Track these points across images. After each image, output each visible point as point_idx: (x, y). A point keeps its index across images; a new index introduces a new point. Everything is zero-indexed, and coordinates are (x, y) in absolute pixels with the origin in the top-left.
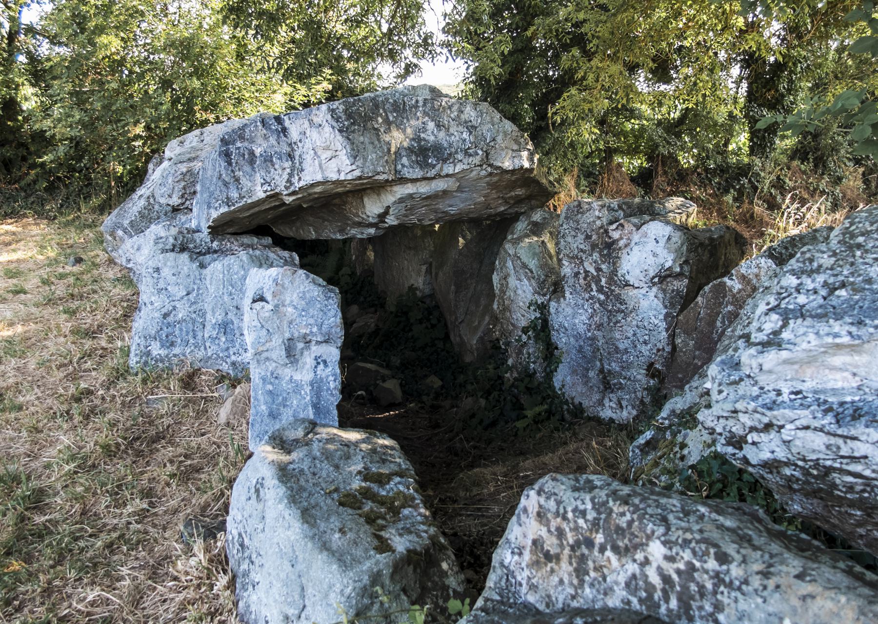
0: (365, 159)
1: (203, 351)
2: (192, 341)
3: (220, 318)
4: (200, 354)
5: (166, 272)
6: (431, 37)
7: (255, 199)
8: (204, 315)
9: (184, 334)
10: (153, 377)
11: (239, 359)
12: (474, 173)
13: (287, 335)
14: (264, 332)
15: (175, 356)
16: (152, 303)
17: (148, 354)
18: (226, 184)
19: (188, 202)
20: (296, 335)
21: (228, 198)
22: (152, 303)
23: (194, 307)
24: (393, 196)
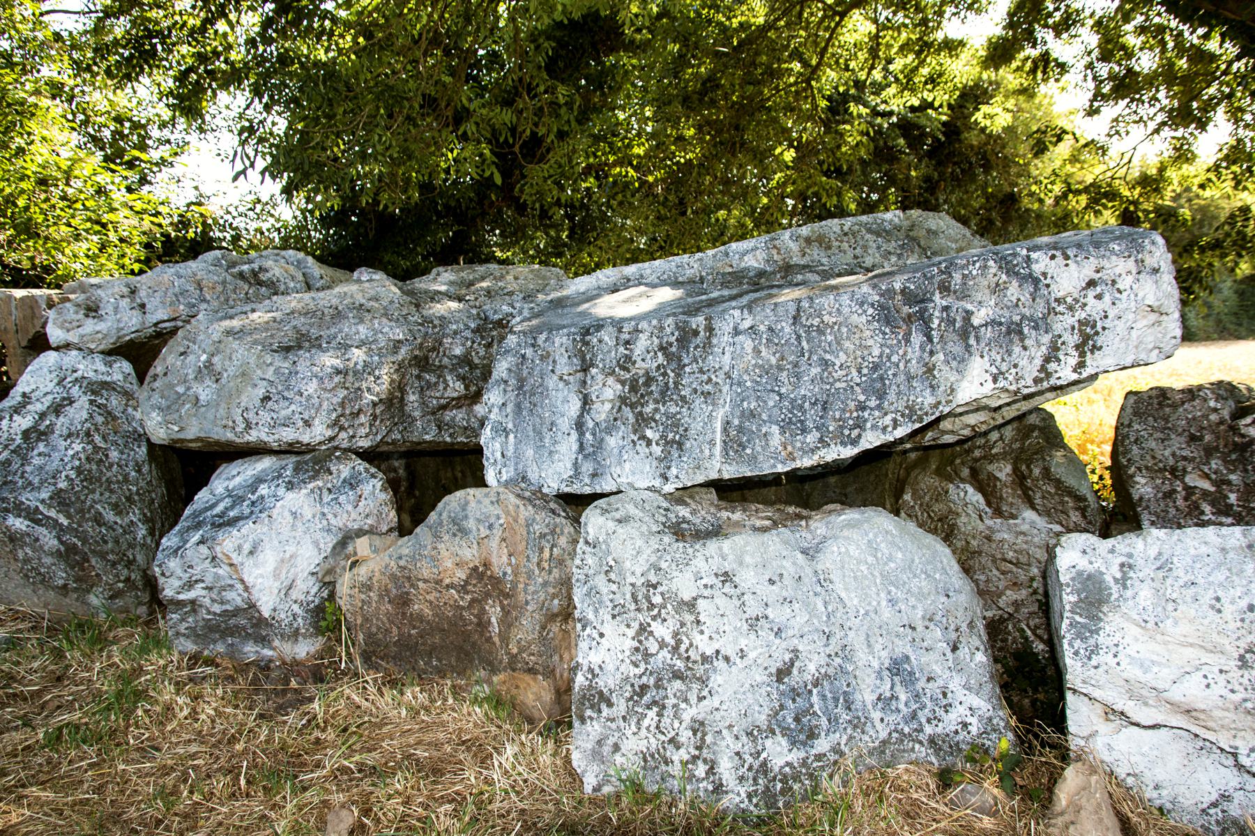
2: (845, 717)
11: (939, 730)
15: (819, 757)
16: (742, 654)
19: (343, 435)
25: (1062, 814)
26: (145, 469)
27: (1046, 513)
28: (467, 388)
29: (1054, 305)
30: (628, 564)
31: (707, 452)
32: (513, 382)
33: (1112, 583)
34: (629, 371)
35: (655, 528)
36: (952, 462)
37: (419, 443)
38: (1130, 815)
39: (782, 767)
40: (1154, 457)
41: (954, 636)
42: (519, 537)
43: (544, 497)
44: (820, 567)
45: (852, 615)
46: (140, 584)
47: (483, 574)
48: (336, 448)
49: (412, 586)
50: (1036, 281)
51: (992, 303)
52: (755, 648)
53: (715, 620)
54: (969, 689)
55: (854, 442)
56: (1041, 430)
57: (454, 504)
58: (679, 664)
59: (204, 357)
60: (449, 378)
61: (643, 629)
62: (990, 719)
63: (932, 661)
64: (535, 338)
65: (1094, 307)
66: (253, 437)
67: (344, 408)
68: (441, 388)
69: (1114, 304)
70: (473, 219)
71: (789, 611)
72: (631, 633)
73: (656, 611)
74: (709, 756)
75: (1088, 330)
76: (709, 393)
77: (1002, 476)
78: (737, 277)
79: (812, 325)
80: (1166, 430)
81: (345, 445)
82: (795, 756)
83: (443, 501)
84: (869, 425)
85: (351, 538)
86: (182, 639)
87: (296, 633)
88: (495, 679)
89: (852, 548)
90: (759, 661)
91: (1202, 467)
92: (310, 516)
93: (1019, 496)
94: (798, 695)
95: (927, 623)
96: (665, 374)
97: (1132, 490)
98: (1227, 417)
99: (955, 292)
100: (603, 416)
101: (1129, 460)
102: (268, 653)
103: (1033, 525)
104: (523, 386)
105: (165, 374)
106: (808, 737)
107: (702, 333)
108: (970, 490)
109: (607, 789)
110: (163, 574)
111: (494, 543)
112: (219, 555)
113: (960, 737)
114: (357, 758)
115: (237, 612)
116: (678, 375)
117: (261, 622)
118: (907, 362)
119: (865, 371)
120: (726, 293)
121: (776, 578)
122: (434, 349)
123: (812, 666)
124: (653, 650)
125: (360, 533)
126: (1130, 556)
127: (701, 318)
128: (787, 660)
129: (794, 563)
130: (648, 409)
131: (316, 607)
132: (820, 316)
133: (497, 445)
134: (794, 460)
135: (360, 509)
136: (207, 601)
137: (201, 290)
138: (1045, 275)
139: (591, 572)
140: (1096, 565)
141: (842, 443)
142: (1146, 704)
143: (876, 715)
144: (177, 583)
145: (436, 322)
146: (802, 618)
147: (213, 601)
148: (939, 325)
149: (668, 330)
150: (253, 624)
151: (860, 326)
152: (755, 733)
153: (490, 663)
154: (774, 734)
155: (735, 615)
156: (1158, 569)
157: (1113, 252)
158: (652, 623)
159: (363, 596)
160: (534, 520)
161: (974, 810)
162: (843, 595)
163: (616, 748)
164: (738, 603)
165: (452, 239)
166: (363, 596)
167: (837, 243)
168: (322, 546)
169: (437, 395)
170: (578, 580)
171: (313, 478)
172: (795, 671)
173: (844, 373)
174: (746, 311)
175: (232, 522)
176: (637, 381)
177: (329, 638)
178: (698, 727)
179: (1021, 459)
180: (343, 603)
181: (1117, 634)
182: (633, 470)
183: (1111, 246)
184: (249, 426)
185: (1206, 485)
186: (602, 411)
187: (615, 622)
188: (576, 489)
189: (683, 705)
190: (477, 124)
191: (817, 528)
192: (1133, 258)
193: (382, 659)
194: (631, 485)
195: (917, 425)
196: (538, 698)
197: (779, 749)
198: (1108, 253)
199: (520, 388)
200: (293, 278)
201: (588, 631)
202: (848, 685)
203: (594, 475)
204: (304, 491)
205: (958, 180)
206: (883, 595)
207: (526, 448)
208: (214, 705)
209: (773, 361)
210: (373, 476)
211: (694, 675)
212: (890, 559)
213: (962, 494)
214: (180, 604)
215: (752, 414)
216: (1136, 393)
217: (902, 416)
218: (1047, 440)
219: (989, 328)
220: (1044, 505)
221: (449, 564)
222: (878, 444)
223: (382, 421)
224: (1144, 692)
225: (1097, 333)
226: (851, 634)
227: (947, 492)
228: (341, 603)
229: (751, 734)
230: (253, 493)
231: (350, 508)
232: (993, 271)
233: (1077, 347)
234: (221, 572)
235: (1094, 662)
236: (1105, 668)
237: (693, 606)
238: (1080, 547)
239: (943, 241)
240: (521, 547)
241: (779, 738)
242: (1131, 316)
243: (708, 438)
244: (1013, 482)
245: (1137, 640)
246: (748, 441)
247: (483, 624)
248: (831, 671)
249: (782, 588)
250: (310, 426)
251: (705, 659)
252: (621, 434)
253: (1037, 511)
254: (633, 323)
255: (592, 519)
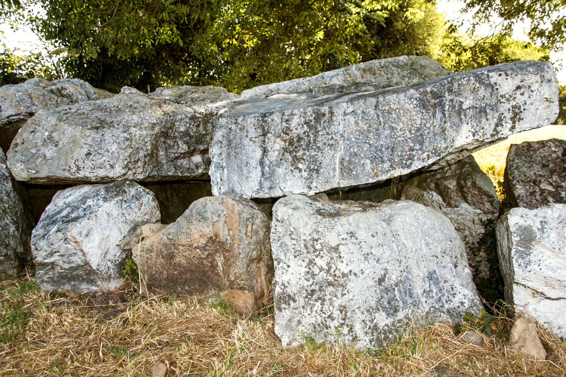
2: (410, 301)
11: (451, 306)
15: (399, 321)
17: (376, 327)
19: (130, 172)
25: (516, 342)
26: (12, 195)
27: (474, 204)
28: (189, 148)
29: (500, 98)
30: (301, 230)
31: (332, 174)
32: (225, 142)
33: (537, 231)
34: (288, 135)
35: (312, 212)
36: (426, 181)
37: (165, 177)
38: (548, 342)
39: (384, 327)
40: (525, 176)
41: (455, 260)
42: (234, 221)
43: (245, 200)
44: (393, 228)
45: (409, 251)
46: (13, 257)
47: (215, 240)
48: (126, 180)
49: (176, 248)
50: (492, 87)
51: (472, 98)
52: (368, 269)
53: (349, 256)
54: (463, 286)
55: (408, 167)
56: (470, 164)
57: (199, 205)
58: (331, 279)
59: (47, 134)
60: (180, 143)
61: (311, 262)
62: (473, 300)
63: (446, 273)
64: (236, 120)
65: (520, 99)
66: (81, 174)
67: (130, 158)
68: (176, 148)
69: (529, 97)
70: (153, 66)
71: (382, 250)
72: (304, 264)
73: (317, 253)
74: (350, 323)
75: (517, 110)
76: (332, 145)
77: (451, 187)
78: (330, 89)
79: (385, 110)
80: (531, 162)
81: (131, 178)
82: (389, 321)
83: (193, 204)
84: (416, 158)
85: (139, 226)
86: (45, 284)
87: (110, 277)
88: (222, 294)
89: (407, 219)
90: (370, 275)
91: (549, 179)
92: (116, 215)
93: (460, 196)
94: (389, 291)
95: (443, 254)
96: (308, 136)
97: (514, 192)
98: (560, 155)
99: (455, 92)
100: (274, 158)
101: (514, 177)
102: (94, 288)
103: (466, 210)
104: (230, 144)
105: (23, 143)
106: (394, 311)
107: (327, 115)
108: (435, 194)
109: (295, 344)
110: (36, 249)
111: (221, 224)
112: (69, 237)
113: (460, 309)
114: (157, 338)
115: (78, 267)
116: (316, 136)
117: (91, 272)
118: (434, 127)
119: (413, 132)
120: (326, 96)
121: (375, 234)
122: (171, 128)
123: (394, 277)
124: (316, 272)
125: (144, 223)
126: (545, 217)
127: (327, 107)
128: (383, 274)
129: (382, 227)
130: (300, 154)
131: (120, 263)
132: (389, 105)
133: (218, 175)
134: (377, 176)
135: (142, 210)
136: (61, 263)
137: (32, 99)
138: (496, 84)
139: (281, 235)
140: (528, 223)
141: (402, 167)
142: (554, 288)
143: (423, 300)
144: (44, 254)
145: (171, 114)
146: (388, 254)
147: (64, 262)
148: (449, 109)
149: (309, 114)
150: (87, 273)
151: (410, 109)
152: (371, 310)
153: (218, 286)
154: (379, 310)
155: (358, 252)
156: (559, 223)
157: (529, 72)
158: (316, 259)
159: (148, 256)
160: (243, 211)
161: (473, 343)
162: (405, 242)
163: (299, 322)
164: (359, 247)
165: (144, 76)
166: (148, 256)
167: (378, 72)
168: (122, 230)
169: (174, 151)
170: (274, 240)
171: (117, 195)
172: (386, 279)
173: (402, 133)
174: (349, 104)
175: (76, 219)
176: (293, 140)
177: (127, 279)
178: (343, 309)
179: (461, 178)
180: (137, 260)
181: (540, 255)
182: (291, 183)
183: (529, 69)
184: (79, 169)
185: (550, 188)
186: (273, 156)
187: (296, 259)
188: (261, 195)
189: (334, 299)
190: (169, 13)
191: (385, 211)
192: (539, 75)
193: (157, 288)
194: (291, 192)
195: (438, 158)
196: (245, 303)
197: (382, 318)
198: (527, 73)
199: (230, 145)
200: (80, 93)
201: (281, 264)
202: (410, 285)
203: (271, 188)
204: (113, 202)
205: (390, 46)
206: (423, 241)
207: (235, 177)
208: (71, 317)
209: (365, 128)
210: (148, 193)
211: (339, 283)
212: (425, 224)
213: (431, 197)
214: (44, 265)
215: (356, 155)
216: (516, 145)
217: (432, 153)
218: (473, 169)
219: (471, 110)
220: (472, 200)
221: (197, 236)
222: (420, 167)
223: (149, 165)
224: (553, 282)
225: (521, 112)
226: (410, 260)
227: (423, 196)
228: (135, 259)
229: (369, 311)
230: (84, 204)
231: (137, 210)
232: (473, 82)
233: (511, 119)
234: (69, 246)
235: (528, 269)
236: (534, 271)
237: (337, 249)
238: (520, 214)
239: (429, 71)
240: (236, 225)
241: (381, 312)
242: (537, 103)
243: (332, 167)
244: (457, 189)
245: (549, 257)
246: (354, 168)
247: (214, 266)
248: (403, 279)
249: (378, 239)
250: (113, 168)
251: (344, 275)
252: (284, 166)
253: (468, 203)
254: (290, 111)
255: (280, 209)
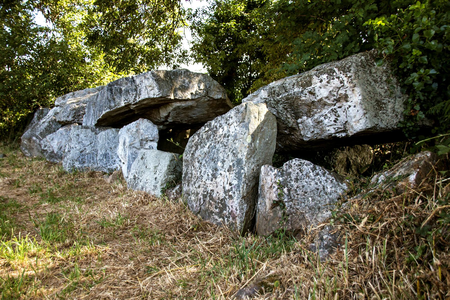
0: (163, 90)
1: (99, 164)
2: (92, 161)
3: (104, 152)
4: (95, 166)
5: (82, 136)
6: (186, 53)
7: (120, 106)
8: (97, 151)
9: (89, 158)
10: (76, 172)
11: (111, 167)
12: (203, 99)
13: (141, 138)
14: (133, 138)
15: (85, 167)
17: (74, 166)
18: (110, 101)
19: (76, 120)
20: (144, 138)
21: (110, 106)
22: (76, 147)
23: (93, 148)
24: (172, 107)
